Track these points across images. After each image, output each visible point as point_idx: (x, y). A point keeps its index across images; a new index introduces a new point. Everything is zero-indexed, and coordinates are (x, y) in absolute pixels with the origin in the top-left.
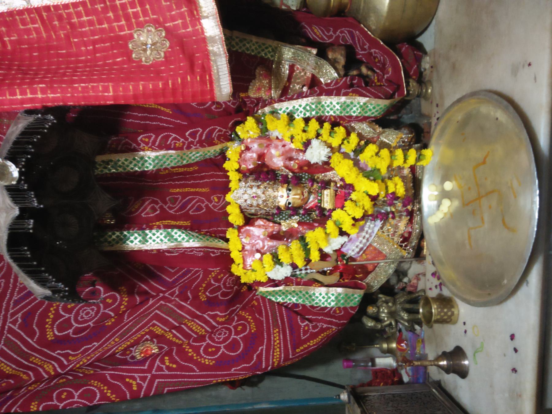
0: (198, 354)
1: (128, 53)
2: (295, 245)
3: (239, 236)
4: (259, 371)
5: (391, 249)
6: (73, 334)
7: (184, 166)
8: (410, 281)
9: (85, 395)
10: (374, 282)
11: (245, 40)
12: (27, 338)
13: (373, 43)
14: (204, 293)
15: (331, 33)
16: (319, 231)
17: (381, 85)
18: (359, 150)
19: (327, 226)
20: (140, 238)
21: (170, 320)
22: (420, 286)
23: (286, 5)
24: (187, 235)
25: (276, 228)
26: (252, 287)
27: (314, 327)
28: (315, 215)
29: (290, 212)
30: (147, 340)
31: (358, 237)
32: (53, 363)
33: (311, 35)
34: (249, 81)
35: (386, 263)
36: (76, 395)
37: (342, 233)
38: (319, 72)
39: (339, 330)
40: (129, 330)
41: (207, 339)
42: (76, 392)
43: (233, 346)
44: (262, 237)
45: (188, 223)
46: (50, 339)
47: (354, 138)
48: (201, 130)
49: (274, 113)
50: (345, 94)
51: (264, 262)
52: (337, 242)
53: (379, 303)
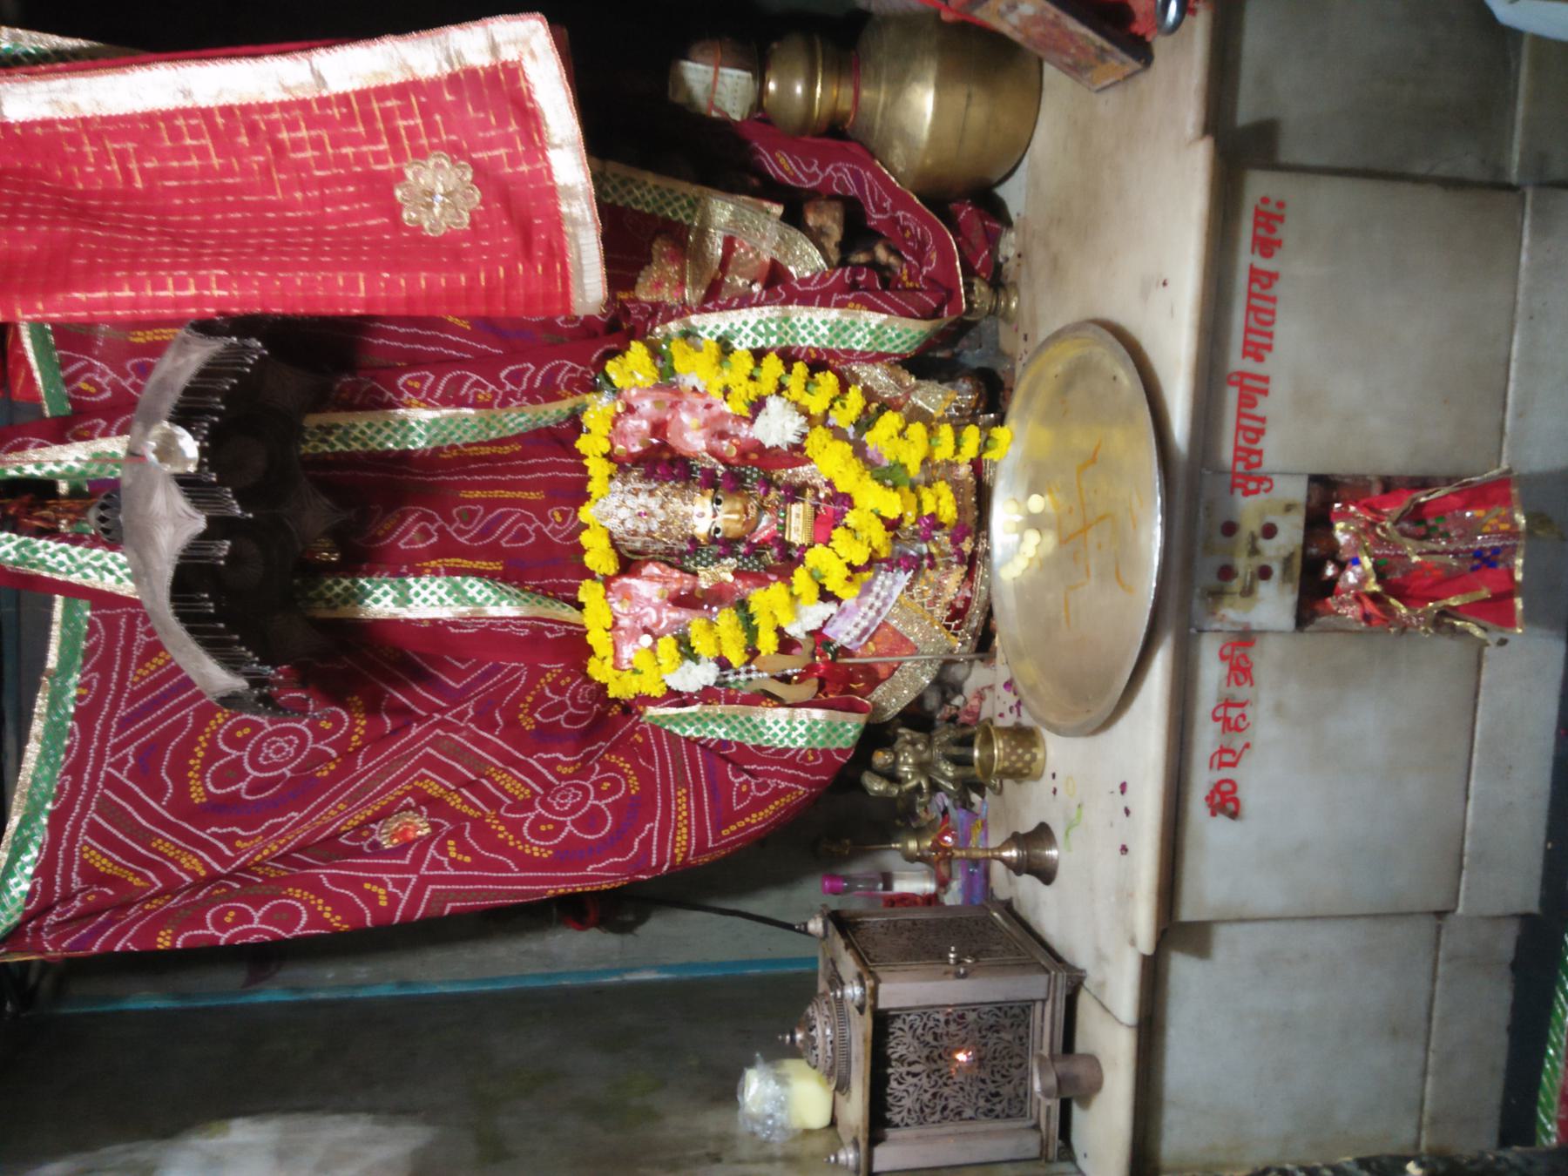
0: (519, 836)
1: (394, 210)
2: (726, 619)
3: (606, 597)
4: (643, 872)
5: (928, 635)
6: (249, 792)
7: (492, 443)
8: (966, 701)
9: (276, 917)
10: (888, 701)
11: (632, 180)
12: (147, 799)
13: (901, 200)
14: (530, 714)
15: (815, 168)
16: (777, 590)
17: (914, 289)
18: (865, 422)
19: (794, 580)
20: (393, 593)
21: (459, 767)
22: (985, 713)
23: (719, 110)
24: (495, 592)
25: (688, 582)
26: (629, 708)
27: (760, 788)
28: (770, 556)
29: (717, 549)
30: (408, 807)
31: (859, 605)
32: (201, 853)
33: (772, 169)
34: (639, 267)
35: (917, 662)
36: (257, 915)
37: (826, 596)
38: (786, 255)
39: (811, 794)
40: (362, 791)
41: (537, 805)
42: (257, 910)
43: (592, 820)
44: (656, 600)
45: (496, 566)
46: (197, 801)
47: (855, 398)
48: (532, 368)
49: (688, 335)
50: (840, 305)
51: (659, 653)
52: (814, 614)
53: (898, 745)
